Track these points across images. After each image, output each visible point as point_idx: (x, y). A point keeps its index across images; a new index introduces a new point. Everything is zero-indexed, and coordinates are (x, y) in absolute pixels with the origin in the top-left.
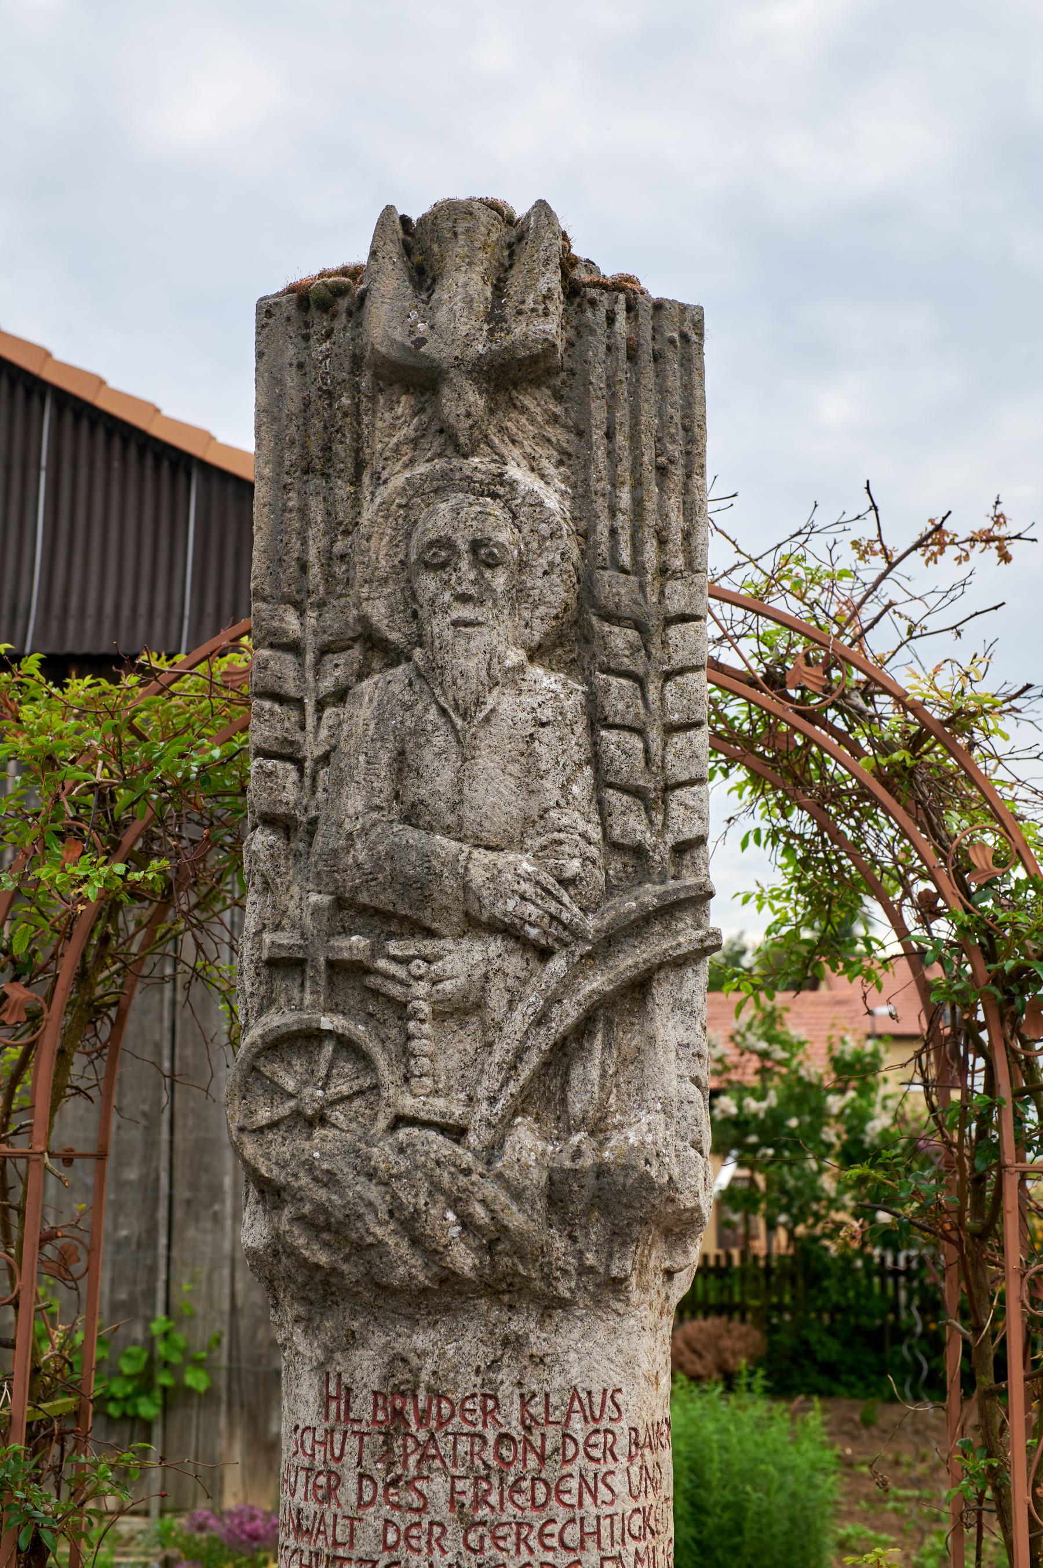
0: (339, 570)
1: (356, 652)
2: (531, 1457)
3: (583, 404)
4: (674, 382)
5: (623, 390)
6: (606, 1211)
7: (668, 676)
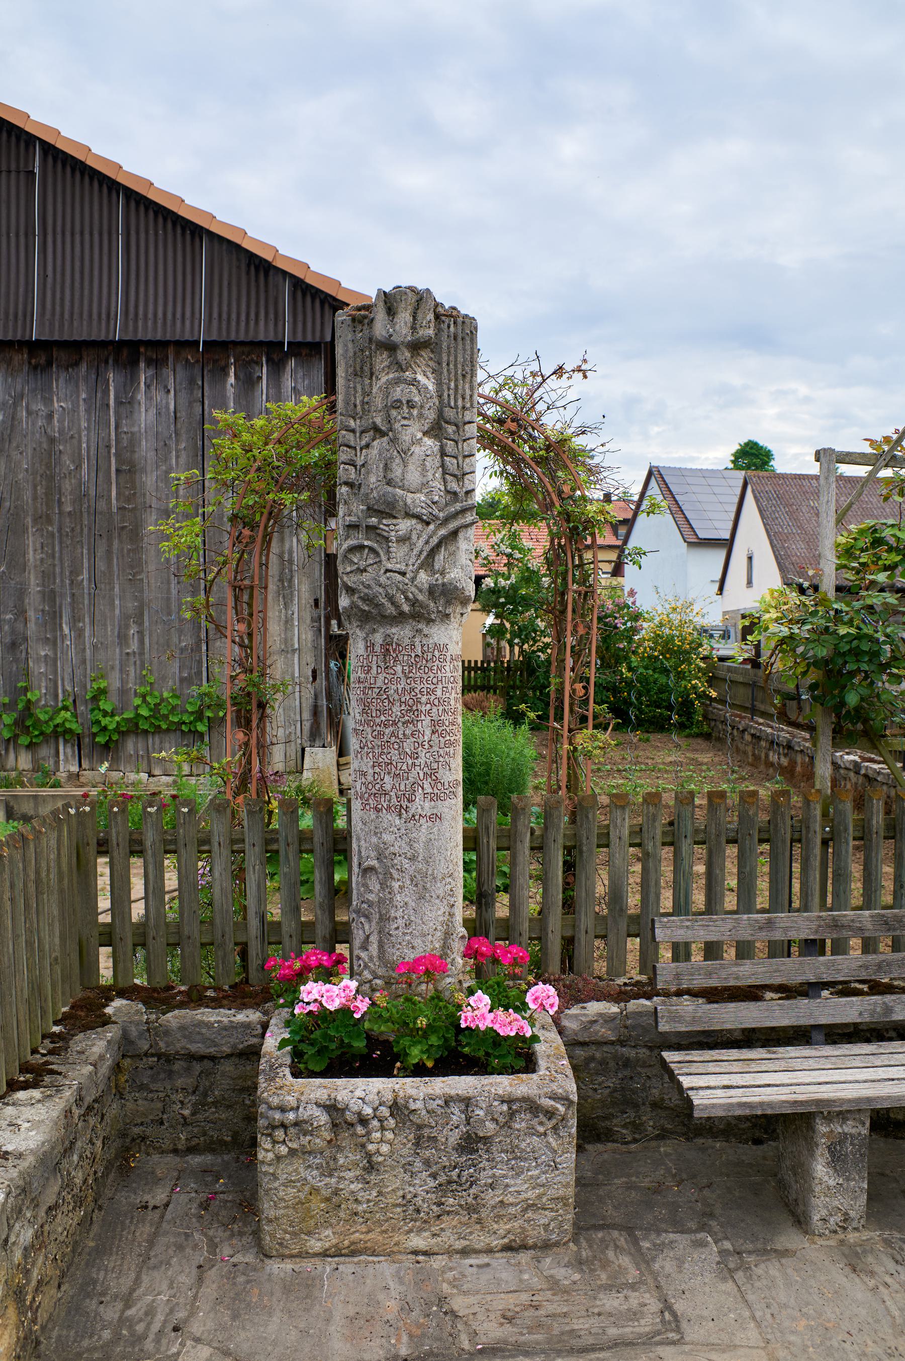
0: (366, 407)
1: (372, 433)
3: (440, 354)
4: (468, 347)
5: (452, 350)
6: (445, 595)
7: (464, 441)
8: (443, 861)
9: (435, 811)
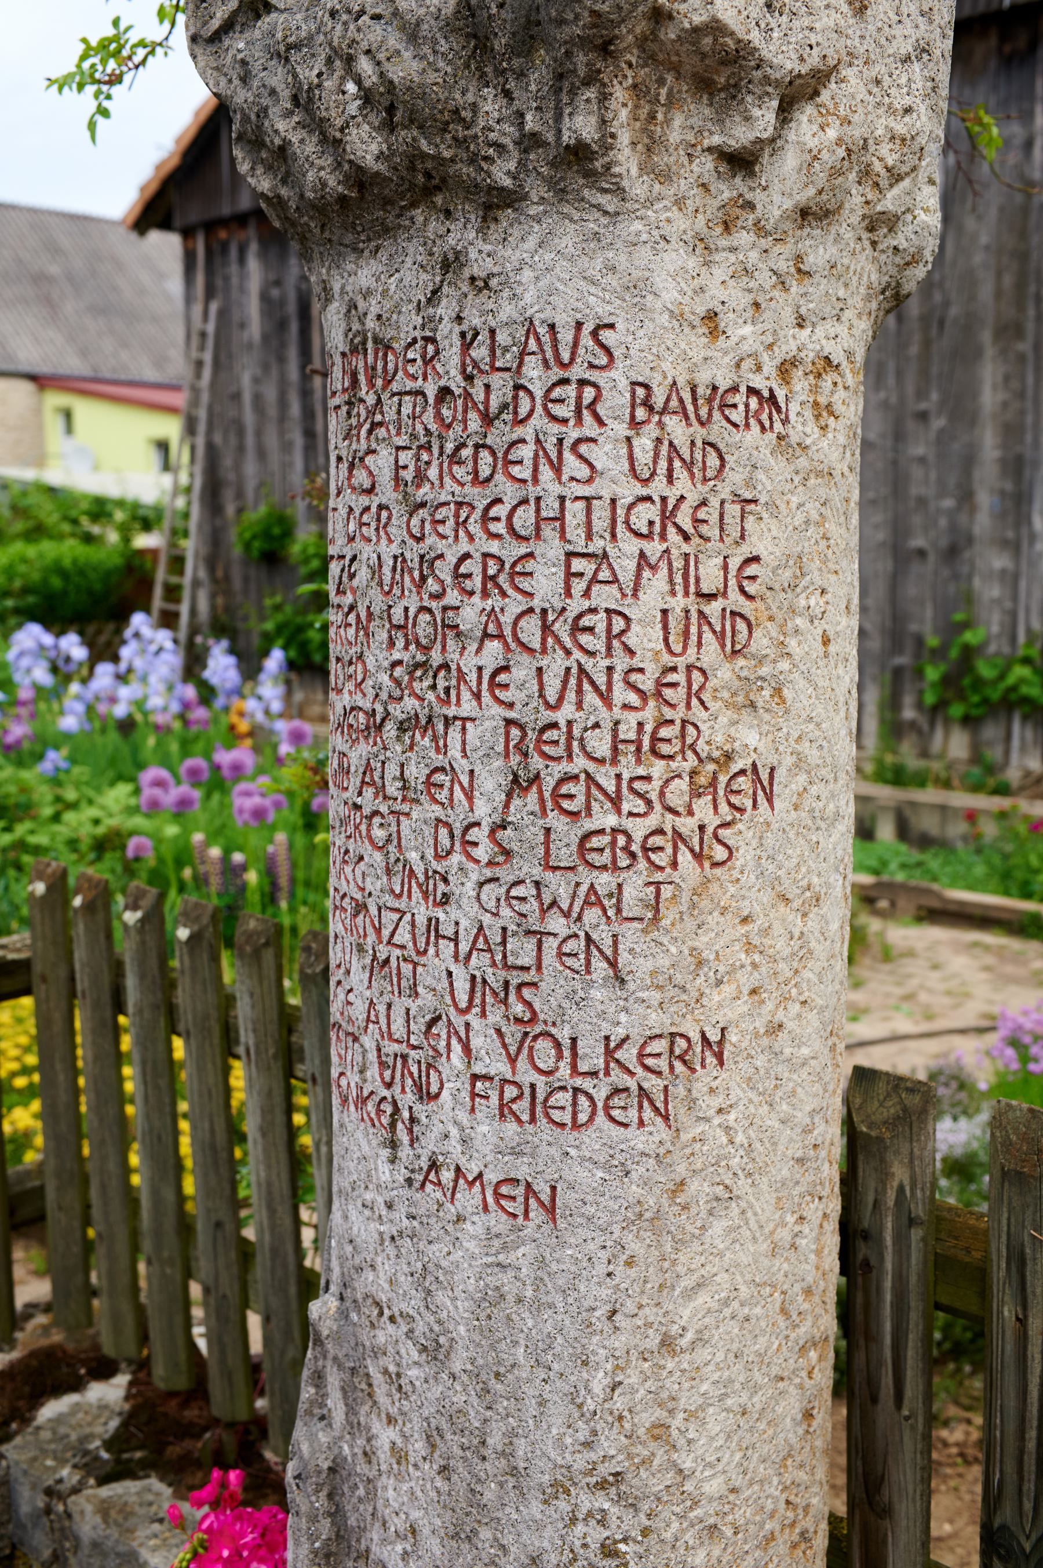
2: (473, 415)
8: (558, 1411)
9: (522, 1171)
